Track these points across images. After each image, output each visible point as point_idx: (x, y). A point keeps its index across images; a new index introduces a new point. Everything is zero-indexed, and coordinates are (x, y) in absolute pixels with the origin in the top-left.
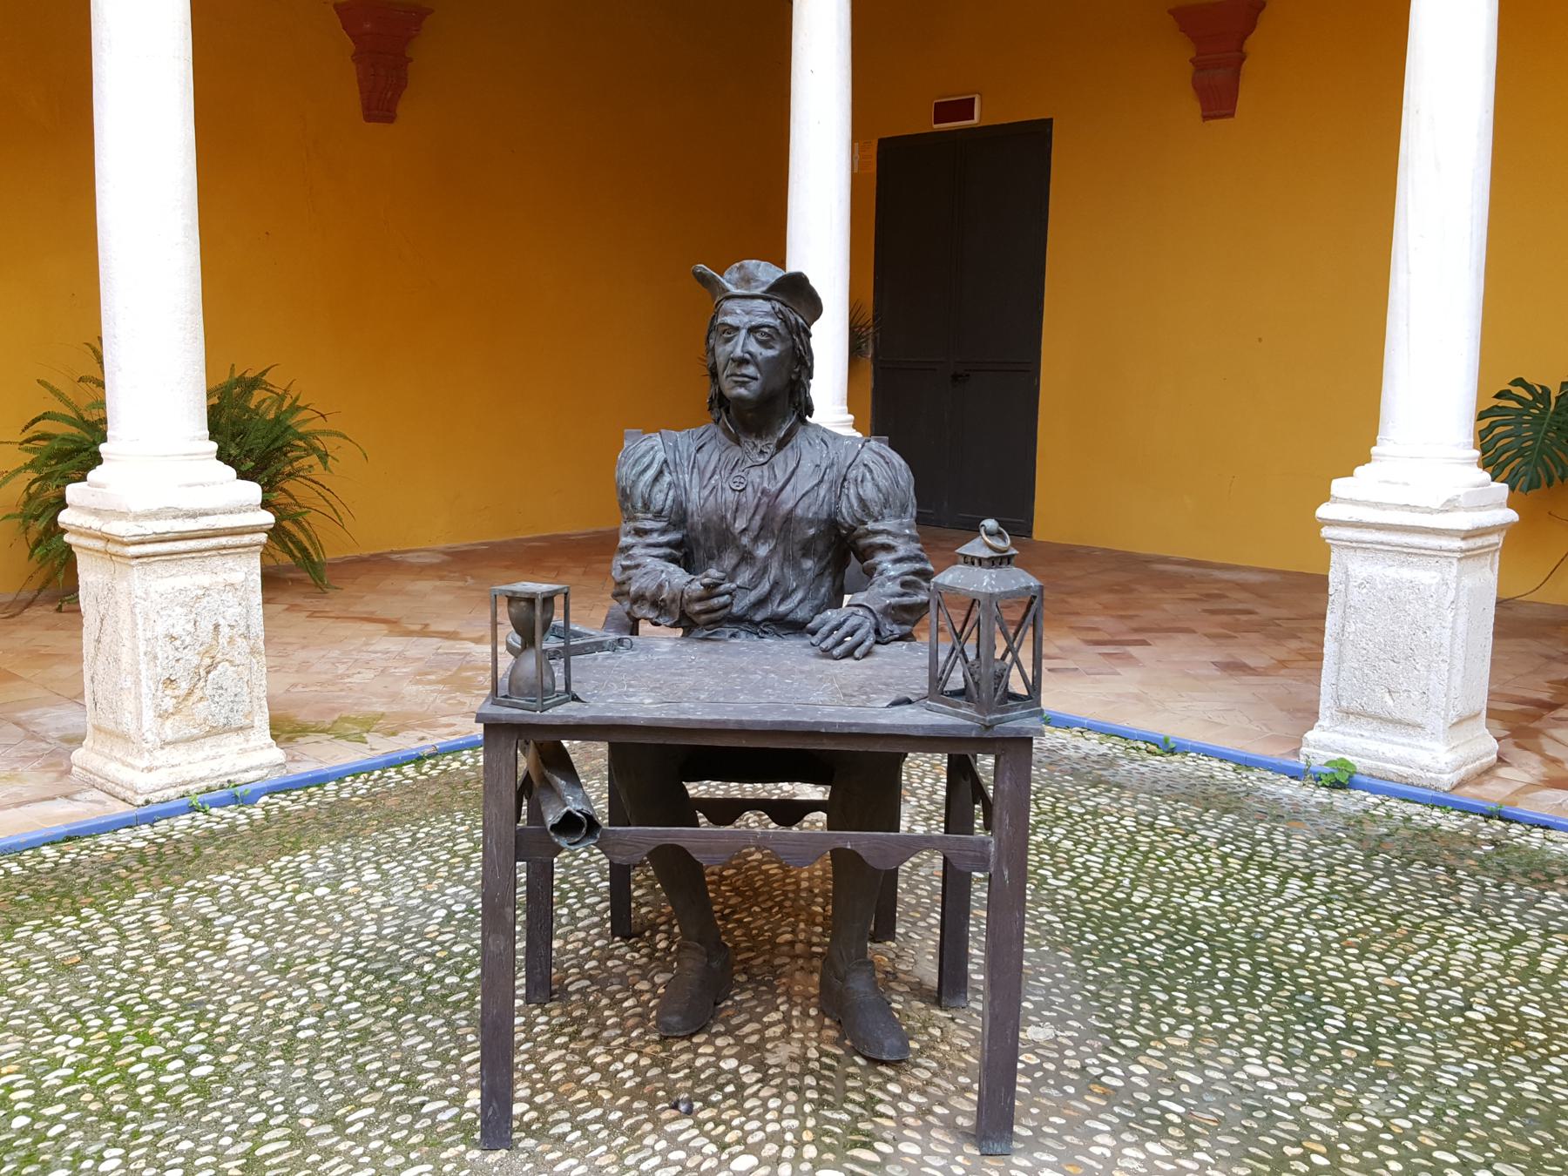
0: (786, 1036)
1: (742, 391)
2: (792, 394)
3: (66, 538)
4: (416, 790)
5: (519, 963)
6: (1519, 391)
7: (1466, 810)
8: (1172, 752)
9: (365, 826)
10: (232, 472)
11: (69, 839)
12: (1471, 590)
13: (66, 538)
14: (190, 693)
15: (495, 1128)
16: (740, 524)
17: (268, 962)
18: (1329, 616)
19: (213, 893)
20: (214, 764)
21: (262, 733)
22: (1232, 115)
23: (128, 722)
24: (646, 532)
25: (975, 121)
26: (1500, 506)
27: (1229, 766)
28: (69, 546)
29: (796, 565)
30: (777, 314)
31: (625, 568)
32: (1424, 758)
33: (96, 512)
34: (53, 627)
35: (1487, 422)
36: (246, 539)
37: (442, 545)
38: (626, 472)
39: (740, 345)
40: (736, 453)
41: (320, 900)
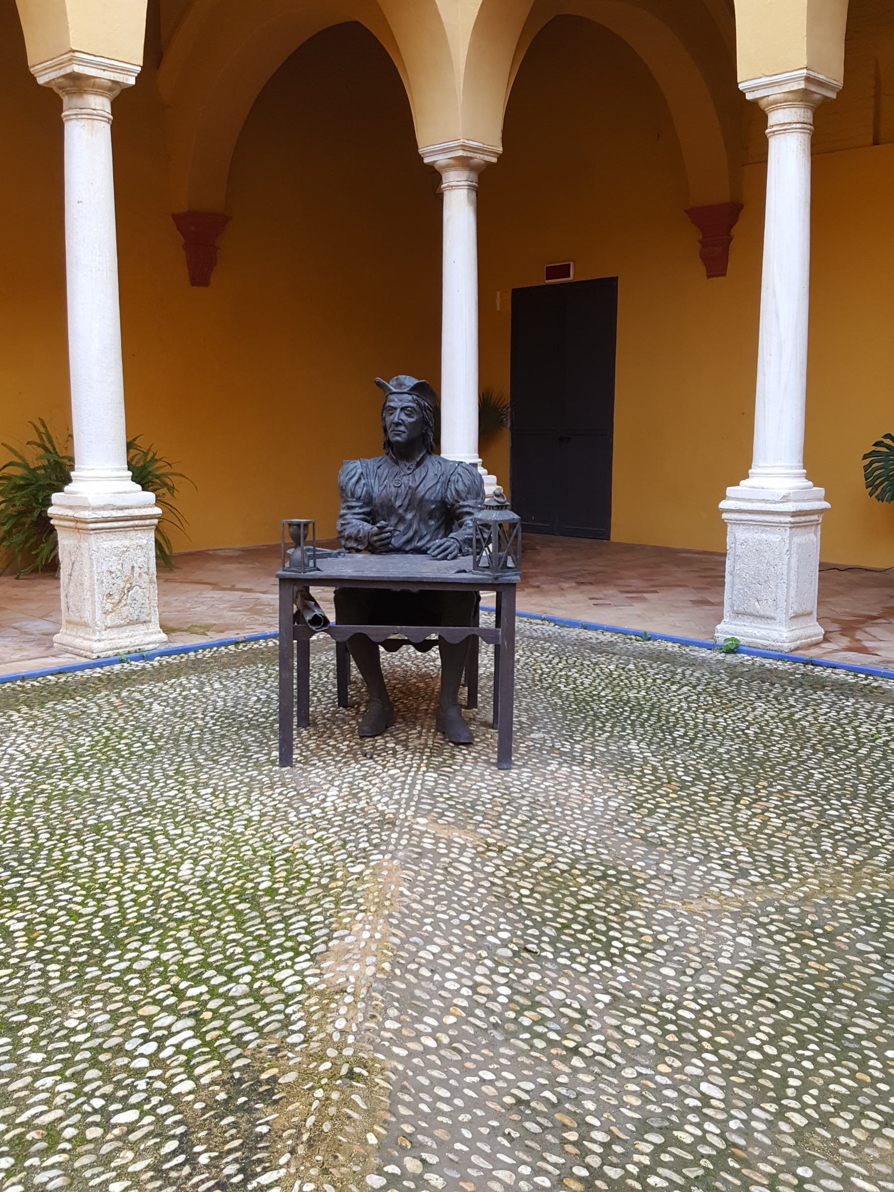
0: (419, 738)
1: (398, 438)
2: (424, 440)
3: (52, 522)
4: (236, 655)
5: (294, 712)
6: (888, 441)
7: (795, 661)
8: (649, 639)
9: (212, 668)
10: (139, 487)
11: (60, 673)
12: (799, 545)
13: (52, 522)
14: (120, 601)
15: (286, 759)
16: (398, 503)
17: (174, 714)
18: (727, 562)
19: (141, 692)
20: (132, 640)
21: (155, 627)
22: (725, 275)
23: (87, 617)
24: (353, 507)
25: (571, 278)
26: (820, 500)
27: (677, 645)
28: (53, 526)
29: (426, 523)
30: (414, 401)
31: (342, 525)
32: (775, 635)
33: (70, 507)
34: (17, 586)
35: (868, 461)
36: (148, 522)
37: (239, 546)
38: (343, 478)
39: (397, 416)
40: (396, 469)
41: (194, 695)
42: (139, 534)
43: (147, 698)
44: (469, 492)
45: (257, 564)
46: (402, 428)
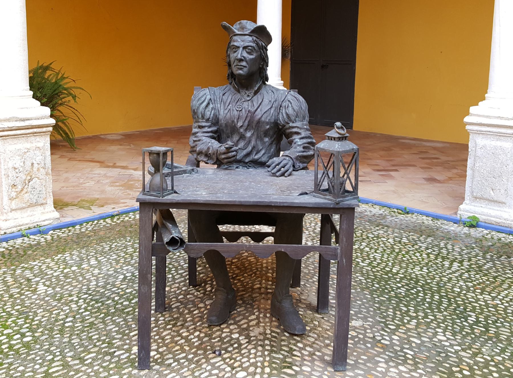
1: (241, 72)
2: (260, 73)
4: (111, 229)
5: (153, 296)
8: (408, 213)
10: (39, 103)
14: (22, 190)
15: (144, 361)
16: (240, 124)
17: (53, 297)
21: (50, 206)
29: (262, 140)
30: (254, 41)
31: (195, 141)
36: (44, 129)
38: (195, 103)
39: (240, 54)
40: (238, 96)
41: (74, 272)
42: (38, 139)
43: (35, 276)
44: (297, 116)
45: (132, 146)
46: (244, 64)
